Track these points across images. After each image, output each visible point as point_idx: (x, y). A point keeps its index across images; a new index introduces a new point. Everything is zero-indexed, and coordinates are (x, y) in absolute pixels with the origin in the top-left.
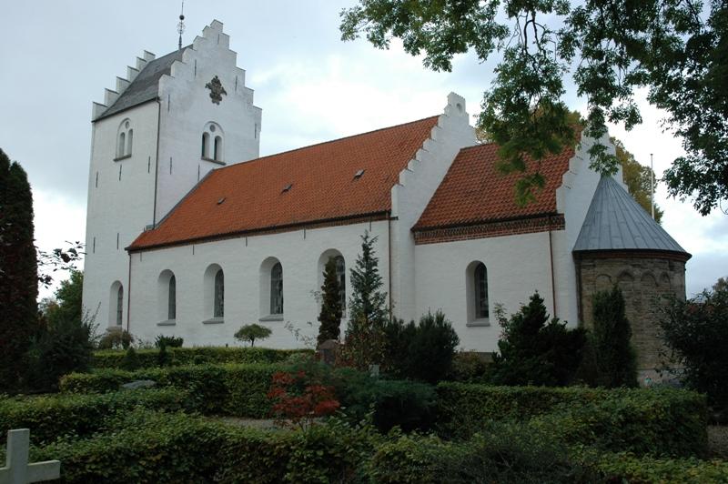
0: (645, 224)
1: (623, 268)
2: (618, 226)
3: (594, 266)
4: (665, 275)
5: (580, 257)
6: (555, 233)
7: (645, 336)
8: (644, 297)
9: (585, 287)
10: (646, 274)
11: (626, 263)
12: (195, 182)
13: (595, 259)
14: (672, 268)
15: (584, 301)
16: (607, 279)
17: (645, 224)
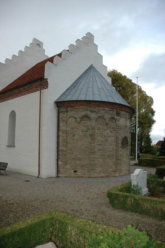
0: (105, 89)
1: (84, 113)
2: (98, 89)
3: (67, 111)
4: (113, 119)
5: (59, 104)
6: (44, 91)
7: (96, 156)
8: (97, 131)
9: (61, 125)
10: (99, 117)
11: (86, 110)
12: (76, 100)
13: (68, 107)
14: (118, 114)
15: (60, 133)
16: (74, 120)
17: (105, 89)
